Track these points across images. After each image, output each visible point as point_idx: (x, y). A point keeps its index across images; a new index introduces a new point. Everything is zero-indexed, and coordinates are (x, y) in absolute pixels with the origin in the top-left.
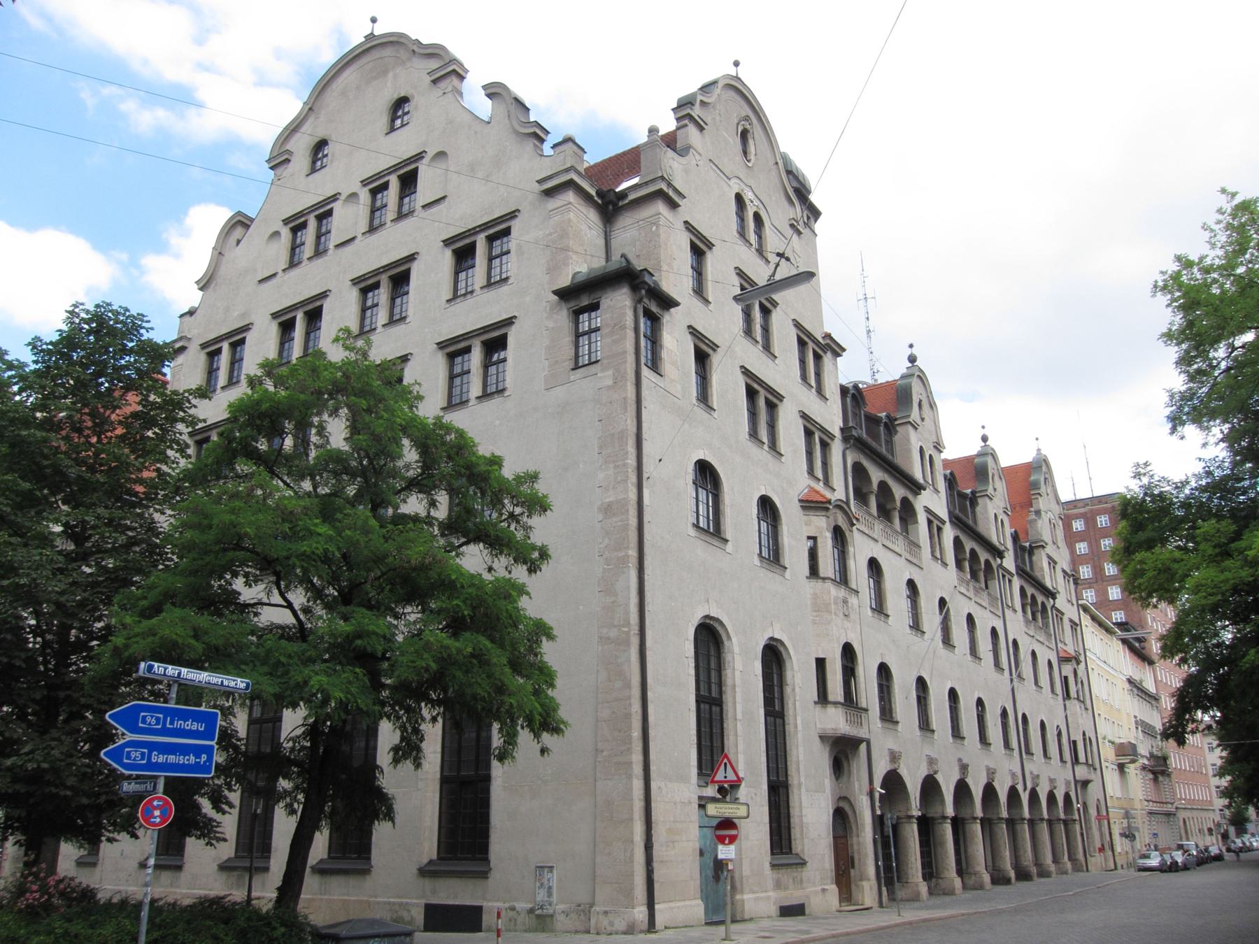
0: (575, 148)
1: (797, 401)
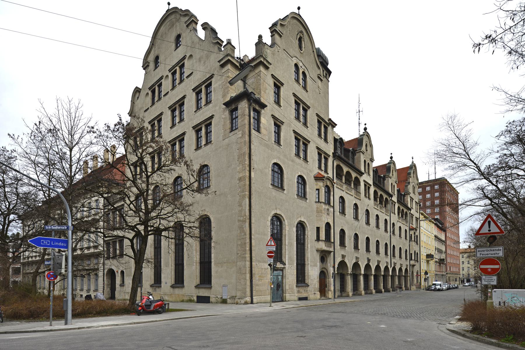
0: (231, 46)
1: (315, 142)
